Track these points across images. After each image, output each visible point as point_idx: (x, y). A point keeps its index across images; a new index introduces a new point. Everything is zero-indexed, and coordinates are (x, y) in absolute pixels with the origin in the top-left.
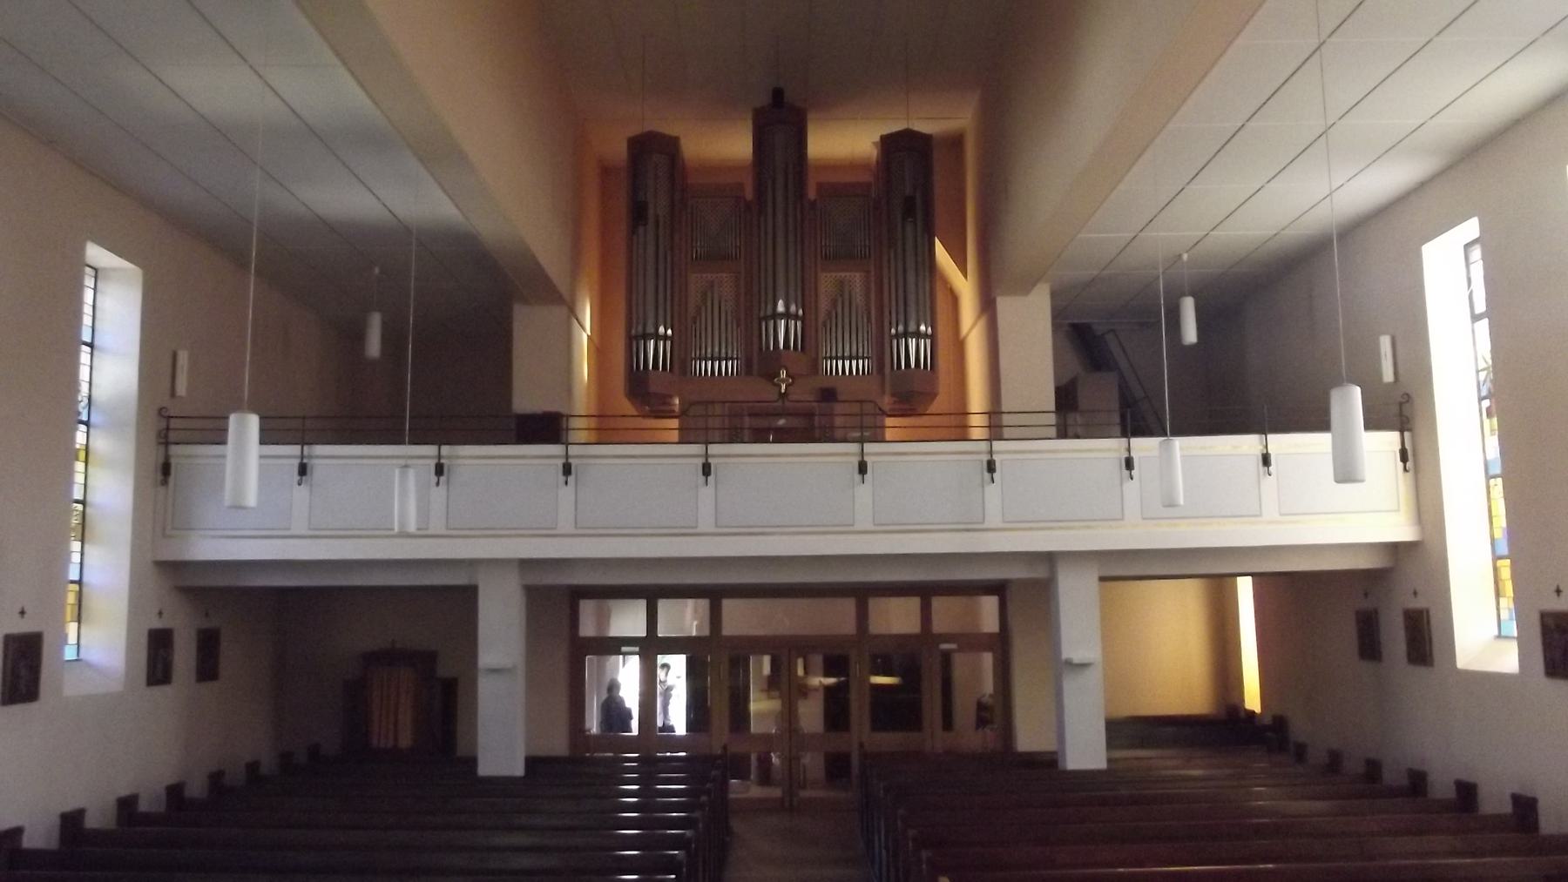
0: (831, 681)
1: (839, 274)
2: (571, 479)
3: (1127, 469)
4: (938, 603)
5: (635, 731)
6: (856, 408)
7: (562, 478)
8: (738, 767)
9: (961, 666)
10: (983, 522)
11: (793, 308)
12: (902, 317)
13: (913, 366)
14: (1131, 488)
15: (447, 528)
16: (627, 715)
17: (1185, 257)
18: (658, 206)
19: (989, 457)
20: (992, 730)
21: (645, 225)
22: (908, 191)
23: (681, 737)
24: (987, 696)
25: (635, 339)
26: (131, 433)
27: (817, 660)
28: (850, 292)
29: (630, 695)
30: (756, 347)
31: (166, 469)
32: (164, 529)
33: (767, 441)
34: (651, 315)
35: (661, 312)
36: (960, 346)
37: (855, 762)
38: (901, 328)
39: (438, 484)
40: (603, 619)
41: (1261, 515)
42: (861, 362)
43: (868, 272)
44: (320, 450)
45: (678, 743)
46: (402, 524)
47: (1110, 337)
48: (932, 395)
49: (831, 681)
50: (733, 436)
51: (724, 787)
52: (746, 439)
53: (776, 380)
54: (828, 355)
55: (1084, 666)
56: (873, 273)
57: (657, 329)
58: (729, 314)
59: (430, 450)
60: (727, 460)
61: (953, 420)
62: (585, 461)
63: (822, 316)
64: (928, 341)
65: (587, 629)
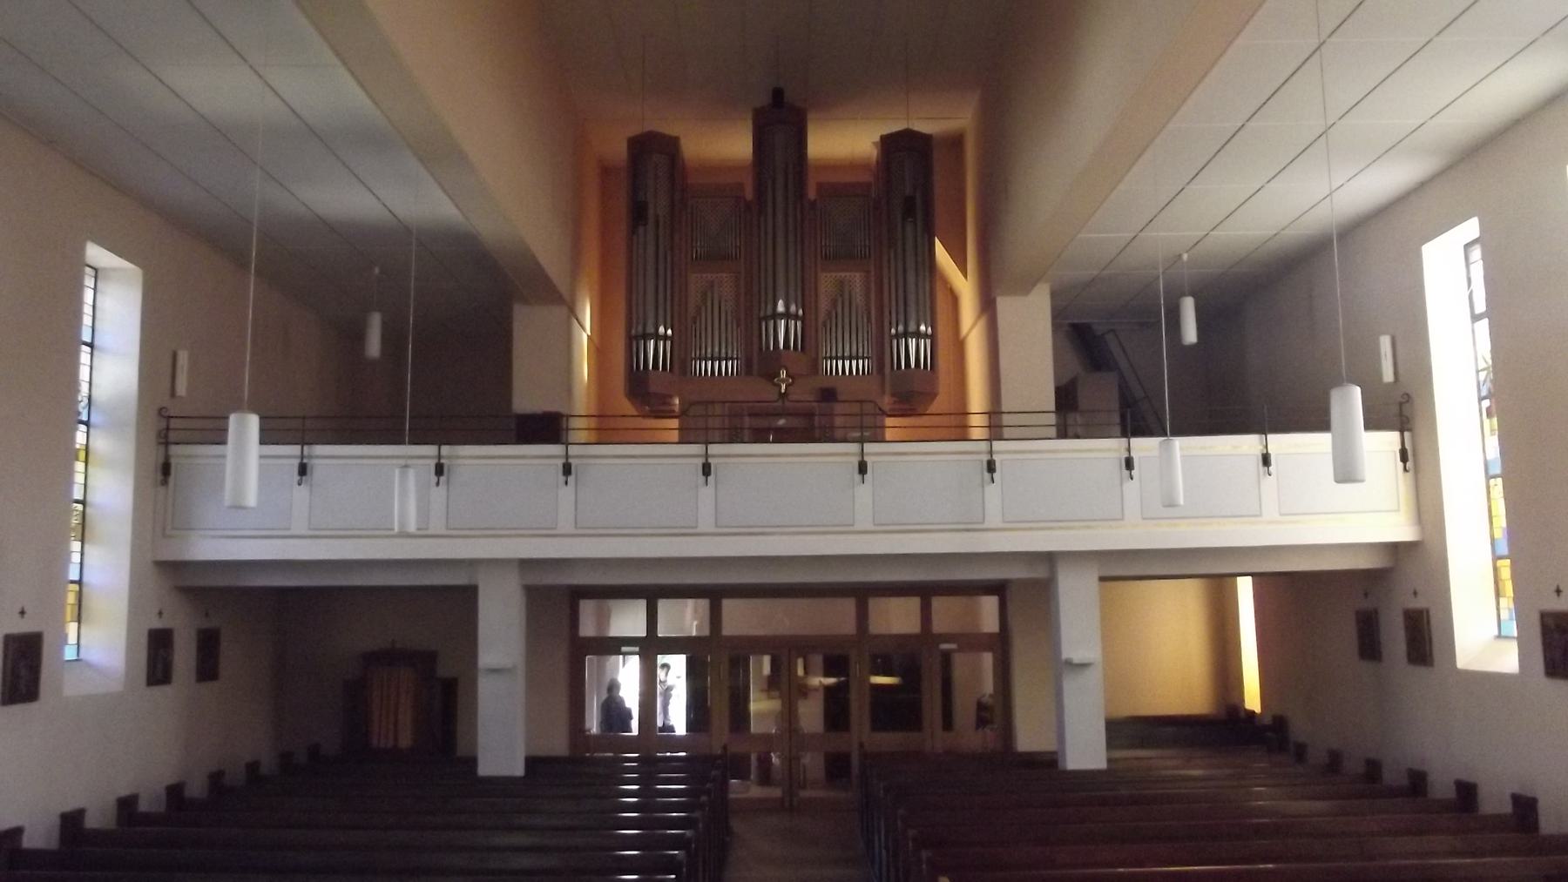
0: (831, 681)
1: (839, 274)
2: (571, 479)
3: (1127, 469)
4: (938, 603)
5: (635, 731)
6: (856, 408)
7: (562, 478)
8: (738, 767)
9: (961, 666)
10: (983, 522)
11: (793, 308)
12: (902, 317)
13: (913, 366)
14: (1131, 488)
15: (447, 528)
16: (627, 715)
17: (1185, 257)
18: (658, 206)
19: (989, 457)
20: (992, 730)
21: (645, 225)
22: (908, 191)
23: (681, 737)
24: (987, 696)
25: (635, 339)
26: (131, 433)
27: (817, 660)
28: (850, 292)
29: (630, 695)
30: (756, 347)
31: (166, 469)
32: (164, 529)
33: (767, 441)
34: (651, 315)
35: (661, 312)
36: (960, 346)
37: (855, 762)
38: (901, 328)
39: (438, 484)
40: (603, 619)
41: (1261, 515)
42: (861, 362)
43: (868, 272)
44: (320, 450)
45: (678, 743)
46: (402, 524)
47: (1110, 337)
48: (932, 395)
49: (831, 681)
50: (733, 436)
51: (724, 787)
52: (746, 439)
53: (776, 380)
54: (828, 355)
55: (1084, 666)
56: (873, 273)
57: (657, 329)
58: (729, 314)
59: (430, 450)
60: (727, 460)
61: (953, 420)
62: (585, 461)
63: (822, 316)
64: (928, 341)
65: (587, 629)
